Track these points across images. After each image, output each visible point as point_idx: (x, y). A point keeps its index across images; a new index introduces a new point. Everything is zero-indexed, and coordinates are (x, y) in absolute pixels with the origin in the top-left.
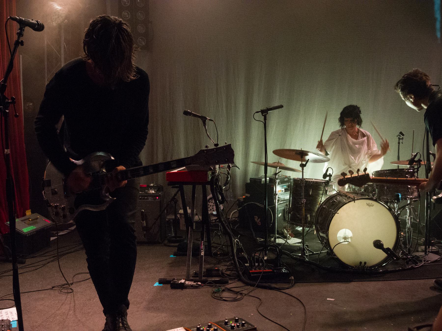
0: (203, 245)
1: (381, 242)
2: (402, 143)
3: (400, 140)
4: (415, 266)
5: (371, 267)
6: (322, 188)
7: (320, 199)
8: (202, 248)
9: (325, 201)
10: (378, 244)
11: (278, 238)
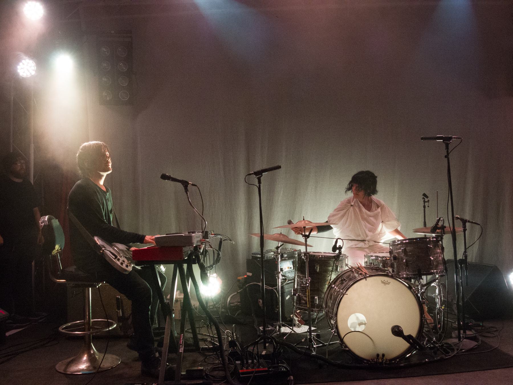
0: (183, 339)
1: (400, 328)
2: (428, 206)
3: (426, 203)
4: (445, 357)
5: (391, 360)
6: (331, 263)
7: (330, 276)
8: (181, 342)
9: (335, 279)
10: (397, 331)
11: (284, 326)
